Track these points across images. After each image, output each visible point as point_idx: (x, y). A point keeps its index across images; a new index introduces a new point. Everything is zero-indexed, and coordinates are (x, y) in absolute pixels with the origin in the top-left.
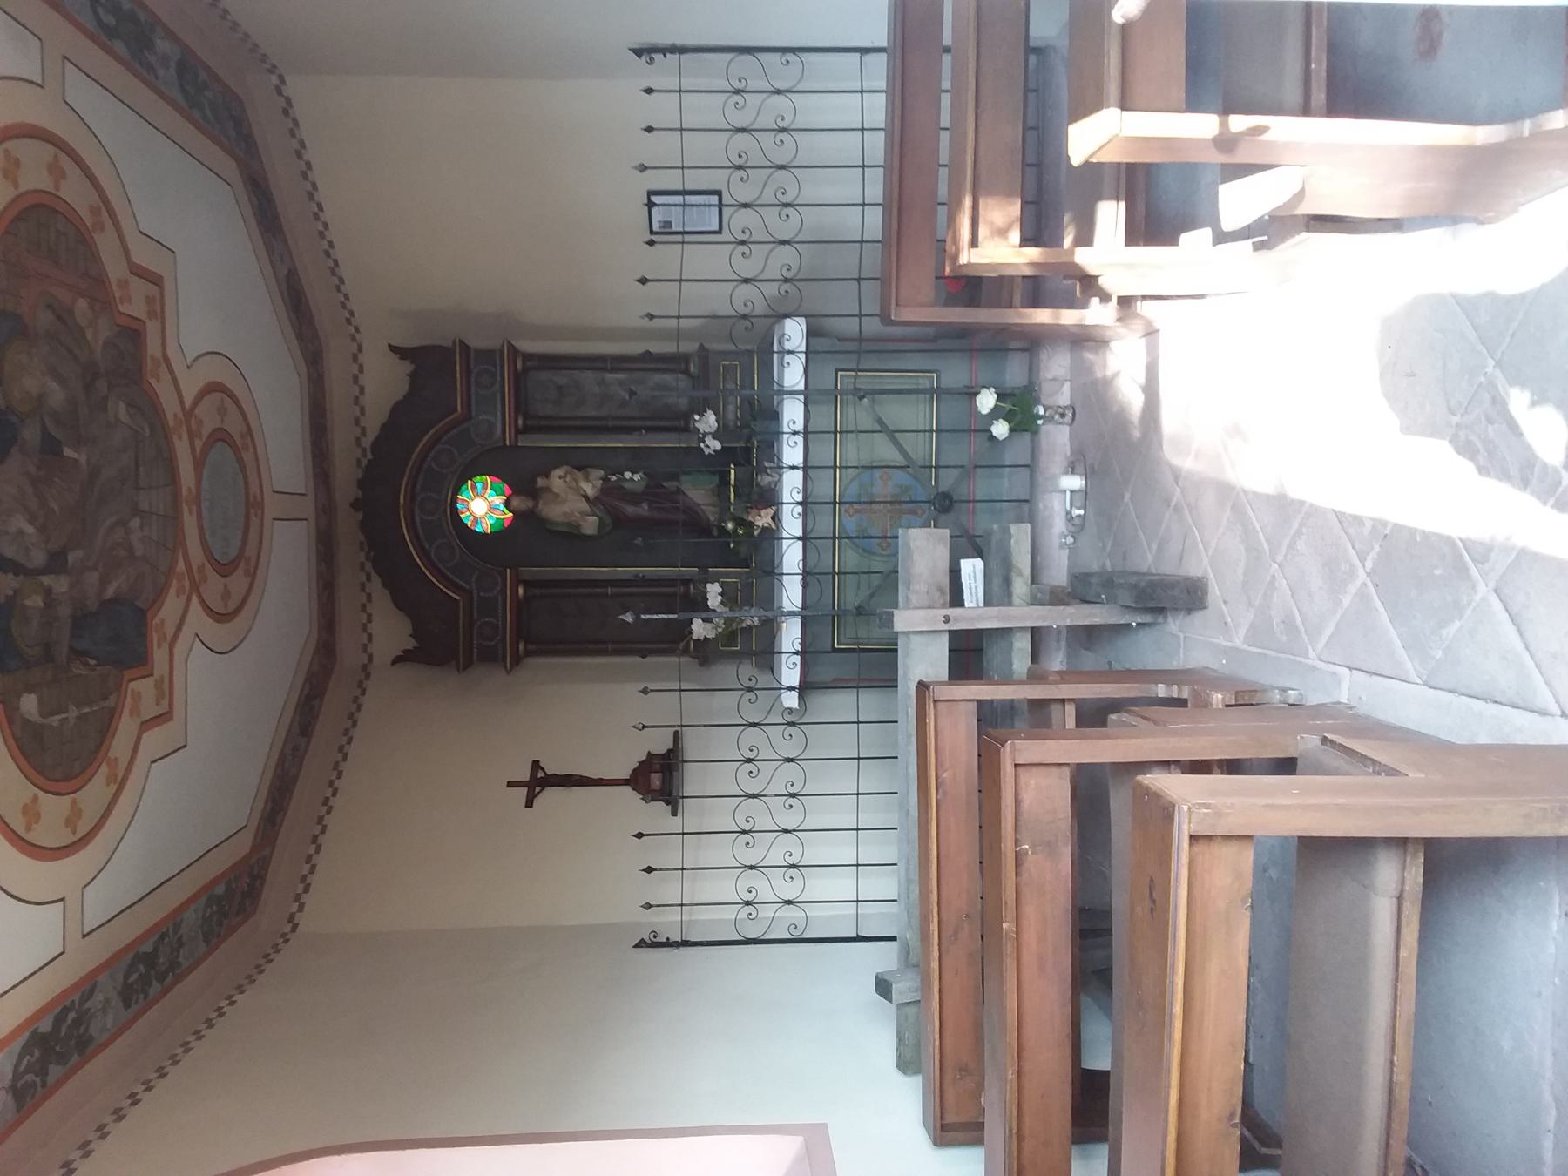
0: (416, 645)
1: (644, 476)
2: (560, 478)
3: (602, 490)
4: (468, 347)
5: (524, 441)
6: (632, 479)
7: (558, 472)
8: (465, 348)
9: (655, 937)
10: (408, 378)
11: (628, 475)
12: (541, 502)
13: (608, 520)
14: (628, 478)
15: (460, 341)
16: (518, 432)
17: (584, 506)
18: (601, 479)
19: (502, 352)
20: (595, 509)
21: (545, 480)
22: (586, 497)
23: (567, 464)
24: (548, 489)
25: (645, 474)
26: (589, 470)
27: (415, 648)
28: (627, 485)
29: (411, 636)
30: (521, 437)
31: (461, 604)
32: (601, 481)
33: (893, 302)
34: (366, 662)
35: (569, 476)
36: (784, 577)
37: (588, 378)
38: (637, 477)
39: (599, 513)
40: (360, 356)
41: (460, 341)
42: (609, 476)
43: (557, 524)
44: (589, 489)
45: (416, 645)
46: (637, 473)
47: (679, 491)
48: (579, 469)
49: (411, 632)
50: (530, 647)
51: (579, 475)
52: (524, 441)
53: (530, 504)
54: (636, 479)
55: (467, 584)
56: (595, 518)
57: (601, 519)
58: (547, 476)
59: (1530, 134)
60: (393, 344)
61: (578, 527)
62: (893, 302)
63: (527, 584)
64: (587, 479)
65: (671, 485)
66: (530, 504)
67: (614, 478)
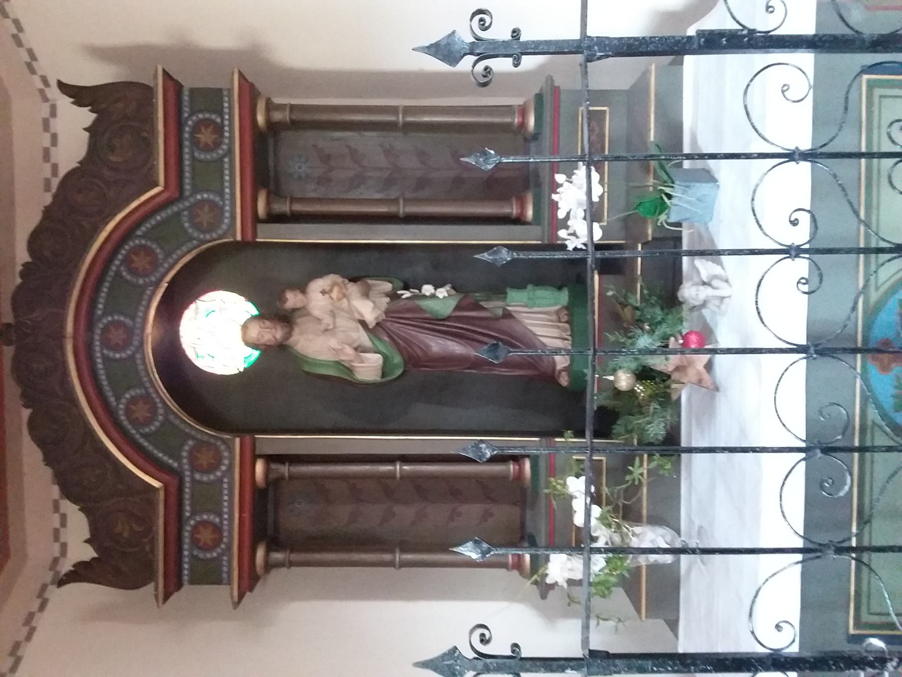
0: (95, 555)
1: (453, 292)
2: (323, 292)
3: (387, 312)
4: (178, 87)
5: (270, 234)
6: (433, 296)
7: (317, 285)
8: (173, 85)
9: (484, 640)
10: (87, 134)
11: (428, 289)
12: (297, 330)
13: (397, 359)
14: (428, 294)
15: (166, 74)
16: (257, 220)
17: (364, 338)
18: (388, 295)
19: (230, 90)
20: (377, 343)
21: (300, 296)
22: (363, 323)
23: (570, 326)
24: (302, 311)
25: (453, 288)
26: (370, 282)
27: (94, 559)
28: (424, 304)
29: (87, 541)
30: (261, 227)
31: (162, 494)
32: (388, 300)
33: (547, 255)
34: (57, 554)
35: (336, 290)
36: (799, 543)
37: (368, 142)
38: (442, 293)
39: (381, 348)
40: (52, 121)
41: (166, 74)
42: (400, 292)
43: (321, 364)
44: (369, 310)
45: (95, 555)
46: (442, 286)
47: (508, 315)
48: (354, 280)
49: (87, 536)
50: (278, 556)
51: (353, 289)
52: (270, 234)
53: (279, 334)
54: (441, 296)
55: (171, 457)
56: (379, 355)
57: (386, 358)
58: (302, 288)
59: (653, 239)
60: (65, 80)
61: (350, 370)
62: (547, 255)
63: (271, 459)
64: (366, 295)
65: (494, 306)
66: (279, 334)
67: (407, 294)
